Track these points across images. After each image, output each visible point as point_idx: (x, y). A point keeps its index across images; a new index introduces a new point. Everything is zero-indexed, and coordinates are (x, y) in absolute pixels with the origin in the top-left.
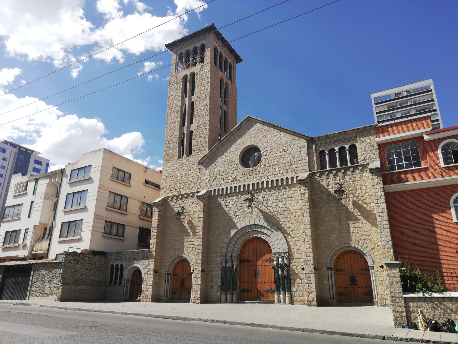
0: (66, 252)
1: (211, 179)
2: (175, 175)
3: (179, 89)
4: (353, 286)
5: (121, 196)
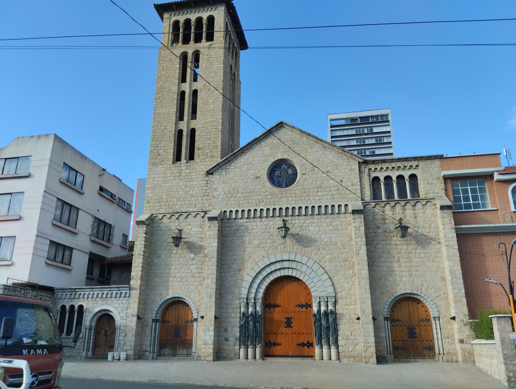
0: (4, 285)
1: (225, 196)
2: (167, 185)
3: (175, 69)
4: (411, 339)
5: (71, 206)
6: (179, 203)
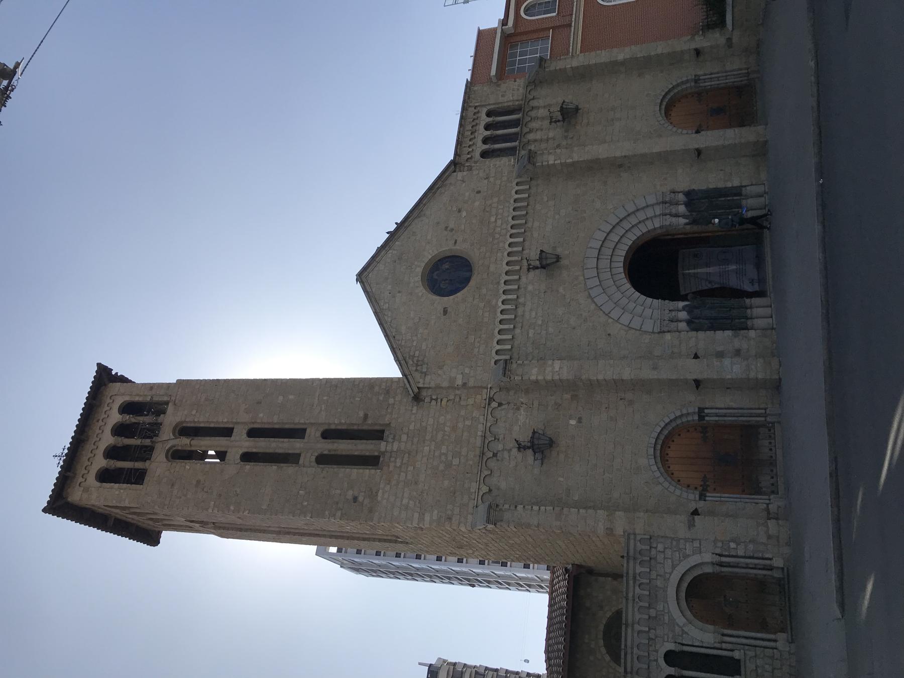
6: (464, 451)
